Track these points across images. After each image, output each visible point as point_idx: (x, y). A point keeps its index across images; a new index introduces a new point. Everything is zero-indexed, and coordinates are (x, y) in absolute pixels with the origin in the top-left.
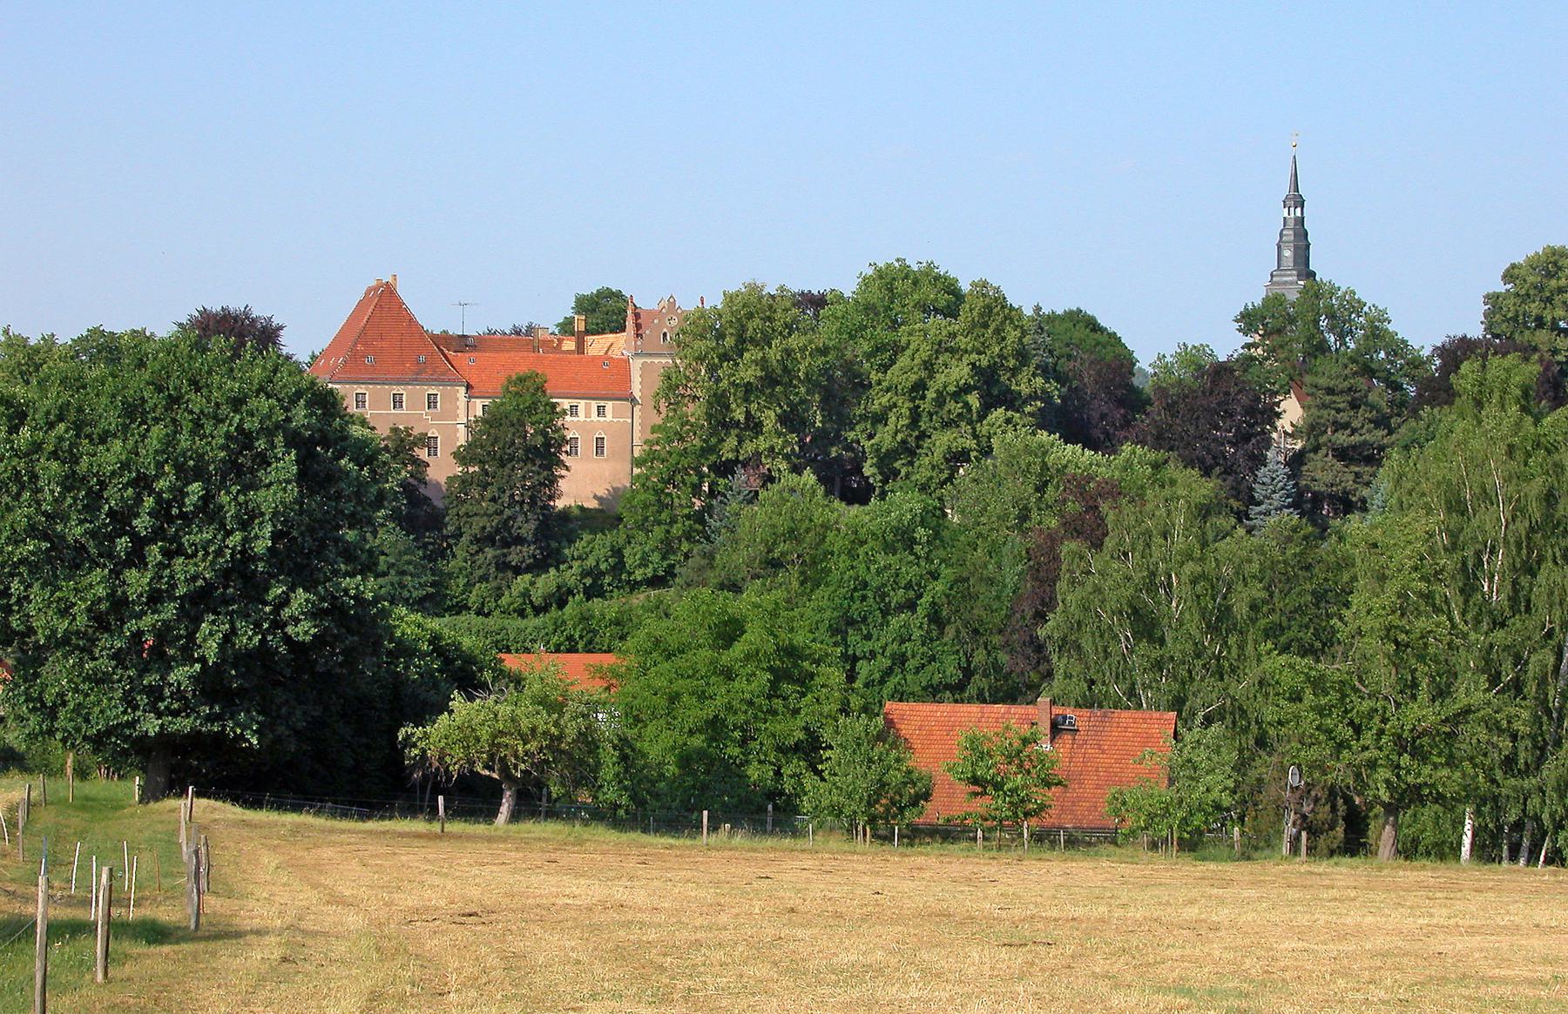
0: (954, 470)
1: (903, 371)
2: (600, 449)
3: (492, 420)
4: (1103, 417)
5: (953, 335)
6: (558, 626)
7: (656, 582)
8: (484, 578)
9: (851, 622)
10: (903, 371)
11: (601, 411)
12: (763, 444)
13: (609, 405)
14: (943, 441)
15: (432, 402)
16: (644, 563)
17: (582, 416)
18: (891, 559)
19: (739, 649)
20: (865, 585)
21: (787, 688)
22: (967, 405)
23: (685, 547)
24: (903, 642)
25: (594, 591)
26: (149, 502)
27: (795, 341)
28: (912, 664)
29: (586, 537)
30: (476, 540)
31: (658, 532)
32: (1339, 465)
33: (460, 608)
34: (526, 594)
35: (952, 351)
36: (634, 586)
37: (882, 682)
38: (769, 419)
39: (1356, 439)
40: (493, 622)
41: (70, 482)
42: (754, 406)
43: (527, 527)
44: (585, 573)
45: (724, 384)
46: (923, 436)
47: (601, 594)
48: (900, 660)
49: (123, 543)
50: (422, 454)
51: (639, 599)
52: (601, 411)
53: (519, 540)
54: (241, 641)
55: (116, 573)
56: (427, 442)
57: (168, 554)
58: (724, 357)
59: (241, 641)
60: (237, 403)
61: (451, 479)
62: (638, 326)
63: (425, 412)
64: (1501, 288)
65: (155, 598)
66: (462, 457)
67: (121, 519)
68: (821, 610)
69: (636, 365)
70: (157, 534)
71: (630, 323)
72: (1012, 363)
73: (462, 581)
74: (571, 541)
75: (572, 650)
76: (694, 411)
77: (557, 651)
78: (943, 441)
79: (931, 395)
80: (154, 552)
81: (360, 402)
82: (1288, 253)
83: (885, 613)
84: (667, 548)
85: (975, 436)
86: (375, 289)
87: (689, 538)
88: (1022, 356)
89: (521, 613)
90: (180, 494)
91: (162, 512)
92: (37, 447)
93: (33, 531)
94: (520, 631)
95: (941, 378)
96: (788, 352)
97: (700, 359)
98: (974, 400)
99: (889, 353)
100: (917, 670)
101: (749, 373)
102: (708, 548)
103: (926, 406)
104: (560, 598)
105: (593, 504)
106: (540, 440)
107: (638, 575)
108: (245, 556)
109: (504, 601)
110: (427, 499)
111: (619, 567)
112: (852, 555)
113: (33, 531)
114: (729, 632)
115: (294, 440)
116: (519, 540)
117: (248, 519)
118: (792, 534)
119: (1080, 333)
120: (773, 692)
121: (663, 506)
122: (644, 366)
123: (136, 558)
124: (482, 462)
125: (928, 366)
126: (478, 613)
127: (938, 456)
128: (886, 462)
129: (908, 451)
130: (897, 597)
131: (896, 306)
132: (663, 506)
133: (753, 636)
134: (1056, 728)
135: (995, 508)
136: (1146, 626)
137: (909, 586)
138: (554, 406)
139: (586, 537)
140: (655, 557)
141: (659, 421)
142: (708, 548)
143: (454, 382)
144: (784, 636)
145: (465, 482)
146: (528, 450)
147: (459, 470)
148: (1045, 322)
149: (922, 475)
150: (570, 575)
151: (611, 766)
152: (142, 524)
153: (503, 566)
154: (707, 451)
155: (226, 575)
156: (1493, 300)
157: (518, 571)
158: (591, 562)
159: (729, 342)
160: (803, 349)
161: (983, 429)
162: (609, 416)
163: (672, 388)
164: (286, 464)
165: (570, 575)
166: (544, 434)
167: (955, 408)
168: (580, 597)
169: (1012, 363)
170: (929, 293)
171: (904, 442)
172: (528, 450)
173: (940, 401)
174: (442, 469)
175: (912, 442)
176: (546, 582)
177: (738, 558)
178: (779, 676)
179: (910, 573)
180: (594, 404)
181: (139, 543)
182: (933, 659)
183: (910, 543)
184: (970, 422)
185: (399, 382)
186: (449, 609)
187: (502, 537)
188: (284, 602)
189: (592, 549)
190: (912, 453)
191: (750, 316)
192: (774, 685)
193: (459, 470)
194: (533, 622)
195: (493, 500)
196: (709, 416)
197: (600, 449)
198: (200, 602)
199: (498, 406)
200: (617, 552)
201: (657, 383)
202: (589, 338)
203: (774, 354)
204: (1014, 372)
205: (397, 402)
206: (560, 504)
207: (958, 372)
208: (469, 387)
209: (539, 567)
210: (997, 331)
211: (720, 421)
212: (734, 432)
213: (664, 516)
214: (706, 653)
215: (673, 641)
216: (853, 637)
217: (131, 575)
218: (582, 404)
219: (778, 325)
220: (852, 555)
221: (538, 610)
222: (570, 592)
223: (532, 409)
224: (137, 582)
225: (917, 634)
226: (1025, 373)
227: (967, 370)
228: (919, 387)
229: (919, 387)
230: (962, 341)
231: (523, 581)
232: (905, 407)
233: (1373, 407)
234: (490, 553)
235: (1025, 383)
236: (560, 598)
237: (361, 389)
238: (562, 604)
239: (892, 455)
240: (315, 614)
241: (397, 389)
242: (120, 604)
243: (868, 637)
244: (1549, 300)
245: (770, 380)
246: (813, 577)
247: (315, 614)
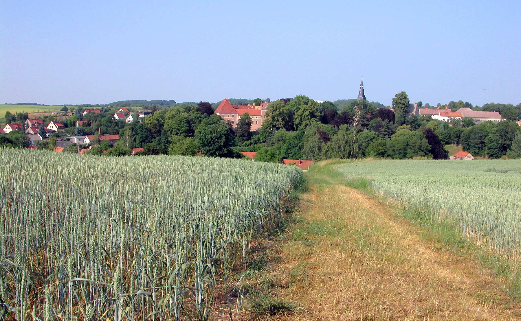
0: (306, 127)
1: (299, 113)
2: (257, 123)
3: (241, 120)
4: (329, 119)
5: (307, 107)
6: (250, 148)
7: (264, 142)
8: (240, 141)
9: (289, 149)
10: (299, 113)
11: (257, 117)
12: (279, 123)
13: (258, 117)
14: (305, 122)
15: (233, 116)
16: (262, 139)
17: (254, 118)
18: (294, 140)
19: (268, 153)
20: (291, 144)
21: (272, 158)
22: (308, 118)
23: (268, 137)
24: (295, 151)
25: (255, 143)
26: (212, 141)
27: (284, 108)
28: (296, 154)
29: (254, 136)
30: (239, 136)
31: (264, 135)
32: (361, 126)
33: (237, 145)
34: (246, 144)
35: (307, 110)
36: (261, 143)
37: (293, 156)
38: (280, 119)
39: (364, 123)
40: (241, 148)
41: (205, 139)
42: (278, 117)
43: (246, 134)
44: (254, 141)
45: (274, 114)
46: (302, 122)
47: (256, 144)
48: (295, 154)
49: (210, 144)
50: (232, 124)
51: (262, 144)
52: (257, 117)
53: (245, 136)
54: (220, 153)
55: (209, 147)
56: (232, 122)
57: (214, 145)
58: (274, 110)
59: (220, 153)
60: (220, 132)
61: (236, 128)
62: (262, 105)
63: (232, 117)
64: (395, 98)
65: (213, 149)
66: (237, 124)
67: (210, 142)
68: (285, 147)
69: (262, 111)
70: (213, 143)
71: (261, 105)
72: (315, 111)
73: (237, 142)
74: (252, 136)
75: (252, 151)
76: (270, 118)
77: (250, 152)
78: (305, 122)
79: (303, 116)
80: (213, 145)
81: (223, 116)
82: (361, 93)
83: (293, 147)
84: (266, 137)
85: (309, 122)
86: (225, 99)
87: (269, 136)
88: (317, 110)
89: (245, 146)
90: (215, 140)
91: (213, 141)
92: (203, 136)
93: (202, 143)
94: (245, 149)
95: (305, 114)
96: (283, 110)
97: (271, 111)
98: (309, 117)
99: (298, 109)
100: (297, 155)
101: (277, 113)
102: (271, 138)
103: (303, 117)
104: (250, 144)
105: (255, 131)
106: (248, 122)
107: (261, 141)
108: (221, 145)
109: (243, 145)
110: (232, 130)
111: (259, 140)
112: (289, 140)
113: (202, 143)
114: (267, 152)
115: (225, 135)
116: (245, 136)
117: (221, 142)
118: (281, 137)
119: (329, 105)
120: (271, 158)
121: (265, 132)
122: (263, 111)
123: (211, 146)
124: (240, 125)
125: (303, 112)
126: (240, 146)
127: (304, 125)
128: (297, 126)
129: (300, 124)
130: (295, 145)
131: (300, 102)
132: (265, 132)
133: (269, 152)
134: (301, 162)
135: (311, 133)
136: (312, 152)
137: (296, 144)
138: (250, 117)
139: (254, 136)
140: (264, 139)
141: (265, 119)
142: (271, 138)
143: (236, 113)
144: (272, 152)
145: (238, 128)
146: (246, 124)
147: (237, 126)
148: (323, 104)
149: (302, 127)
150: (252, 141)
151: (384, 260)
152: (212, 143)
153: (243, 140)
154: (271, 124)
155: (219, 147)
156: (394, 99)
157: (245, 140)
158: (255, 139)
159: (275, 108)
160: (285, 110)
161: (310, 121)
162: (258, 118)
163: (267, 115)
164: (224, 137)
165: (252, 141)
166: (249, 122)
167: (306, 118)
168: (253, 144)
169: (315, 111)
170: (305, 100)
171: (299, 122)
172: (246, 124)
173: (305, 117)
174: (235, 126)
175: (301, 122)
176: (249, 142)
177: (274, 140)
178: (272, 156)
179: (297, 142)
180: (256, 117)
181: (211, 145)
182: (299, 154)
183: (296, 138)
184: (309, 120)
185: (228, 113)
186: (235, 146)
187: (243, 136)
188: (224, 149)
189: (255, 137)
190: (301, 124)
191: (278, 105)
192: (271, 157)
193: (237, 126)
194: (247, 148)
195: (242, 130)
196: (272, 119)
197: (257, 123)
198: (217, 150)
199: (242, 117)
200: (259, 138)
201: (265, 113)
202: (255, 106)
203: (281, 110)
204: (316, 112)
205: (228, 116)
206: (251, 131)
207: (307, 113)
208: (238, 114)
209: (248, 140)
210: (313, 107)
211: (273, 119)
212: (275, 121)
213: (265, 133)
214: (264, 154)
215: (261, 153)
216: (289, 151)
217: (211, 147)
218: (254, 116)
219: (282, 106)
220: (289, 140)
221: (248, 146)
222: (252, 144)
223: (247, 118)
224: (211, 148)
225: (297, 150)
226: (317, 113)
227: (309, 112)
228: (302, 115)
229: (302, 115)
230: (308, 108)
231: (246, 142)
232: (300, 117)
233: (367, 118)
234: (241, 138)
235: (318, 114)
236: (250, 144)
237: (223, 114)
238: (251, 145)
239: (298, 124)
240: (227, 151)
241: (228, 114)
242: (210, 150)
243: (291, 151)
244: (402, 100)
245: (281, 114)
246: (284, 142)
247: (227, 151)
